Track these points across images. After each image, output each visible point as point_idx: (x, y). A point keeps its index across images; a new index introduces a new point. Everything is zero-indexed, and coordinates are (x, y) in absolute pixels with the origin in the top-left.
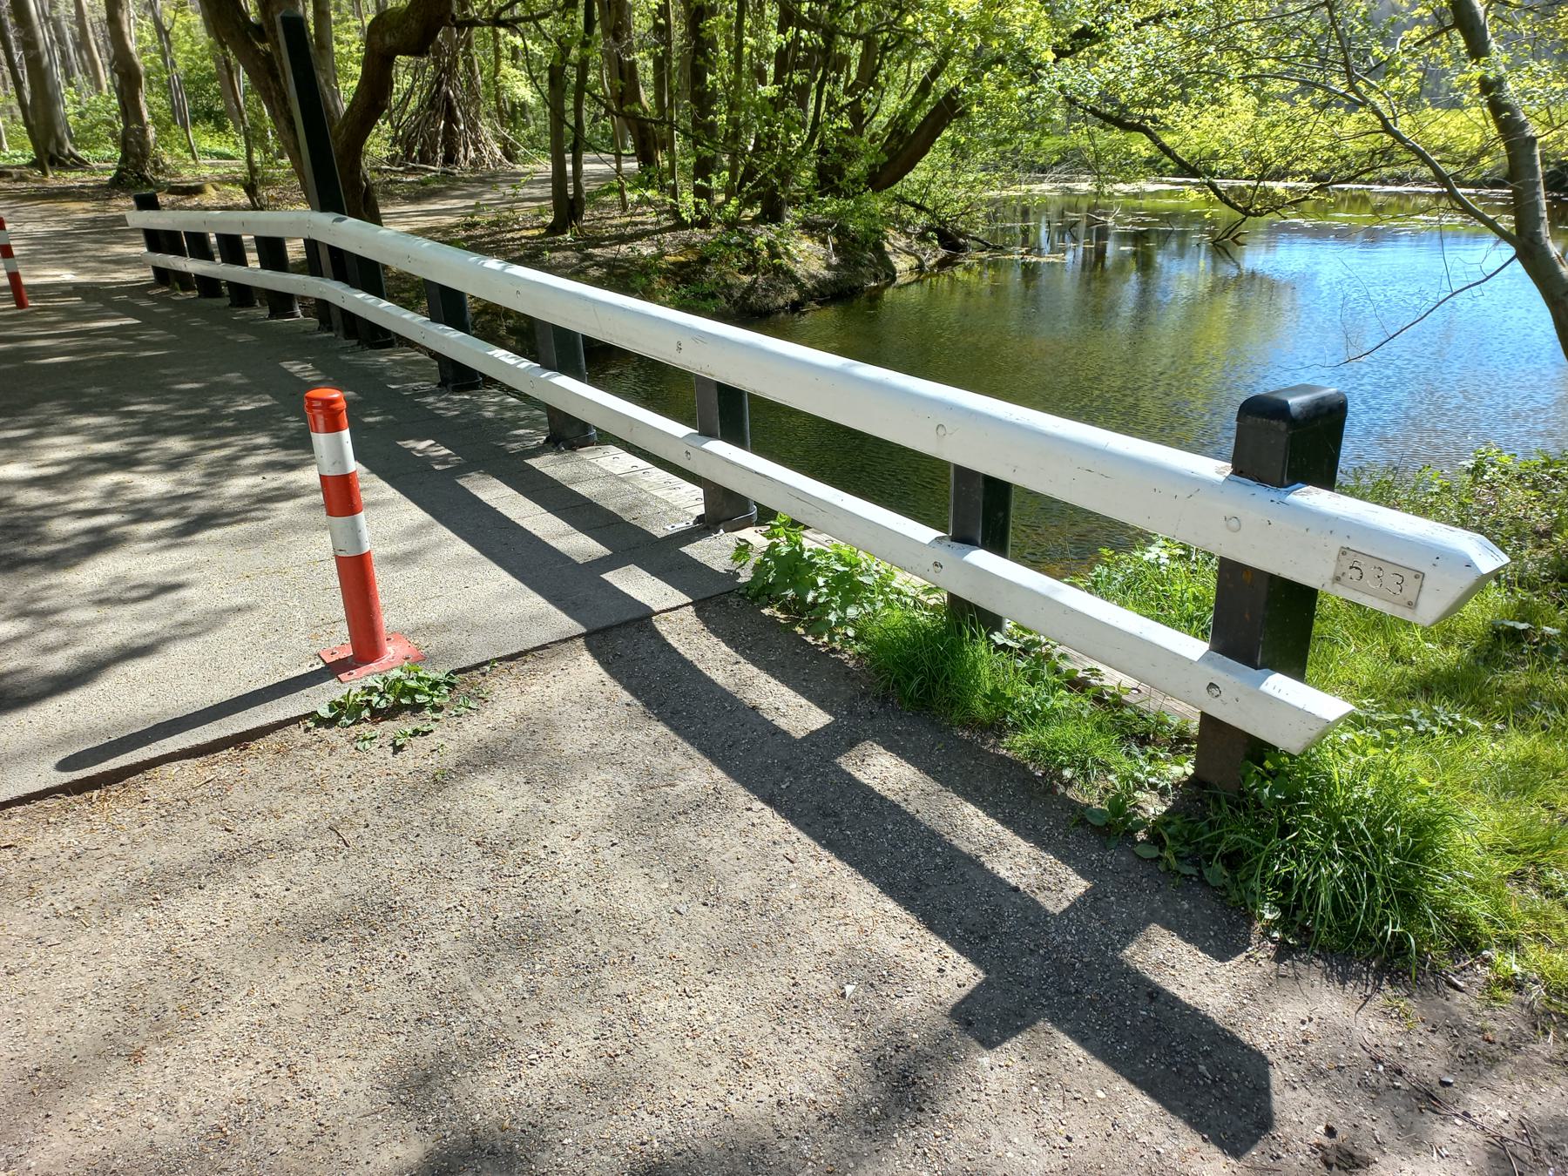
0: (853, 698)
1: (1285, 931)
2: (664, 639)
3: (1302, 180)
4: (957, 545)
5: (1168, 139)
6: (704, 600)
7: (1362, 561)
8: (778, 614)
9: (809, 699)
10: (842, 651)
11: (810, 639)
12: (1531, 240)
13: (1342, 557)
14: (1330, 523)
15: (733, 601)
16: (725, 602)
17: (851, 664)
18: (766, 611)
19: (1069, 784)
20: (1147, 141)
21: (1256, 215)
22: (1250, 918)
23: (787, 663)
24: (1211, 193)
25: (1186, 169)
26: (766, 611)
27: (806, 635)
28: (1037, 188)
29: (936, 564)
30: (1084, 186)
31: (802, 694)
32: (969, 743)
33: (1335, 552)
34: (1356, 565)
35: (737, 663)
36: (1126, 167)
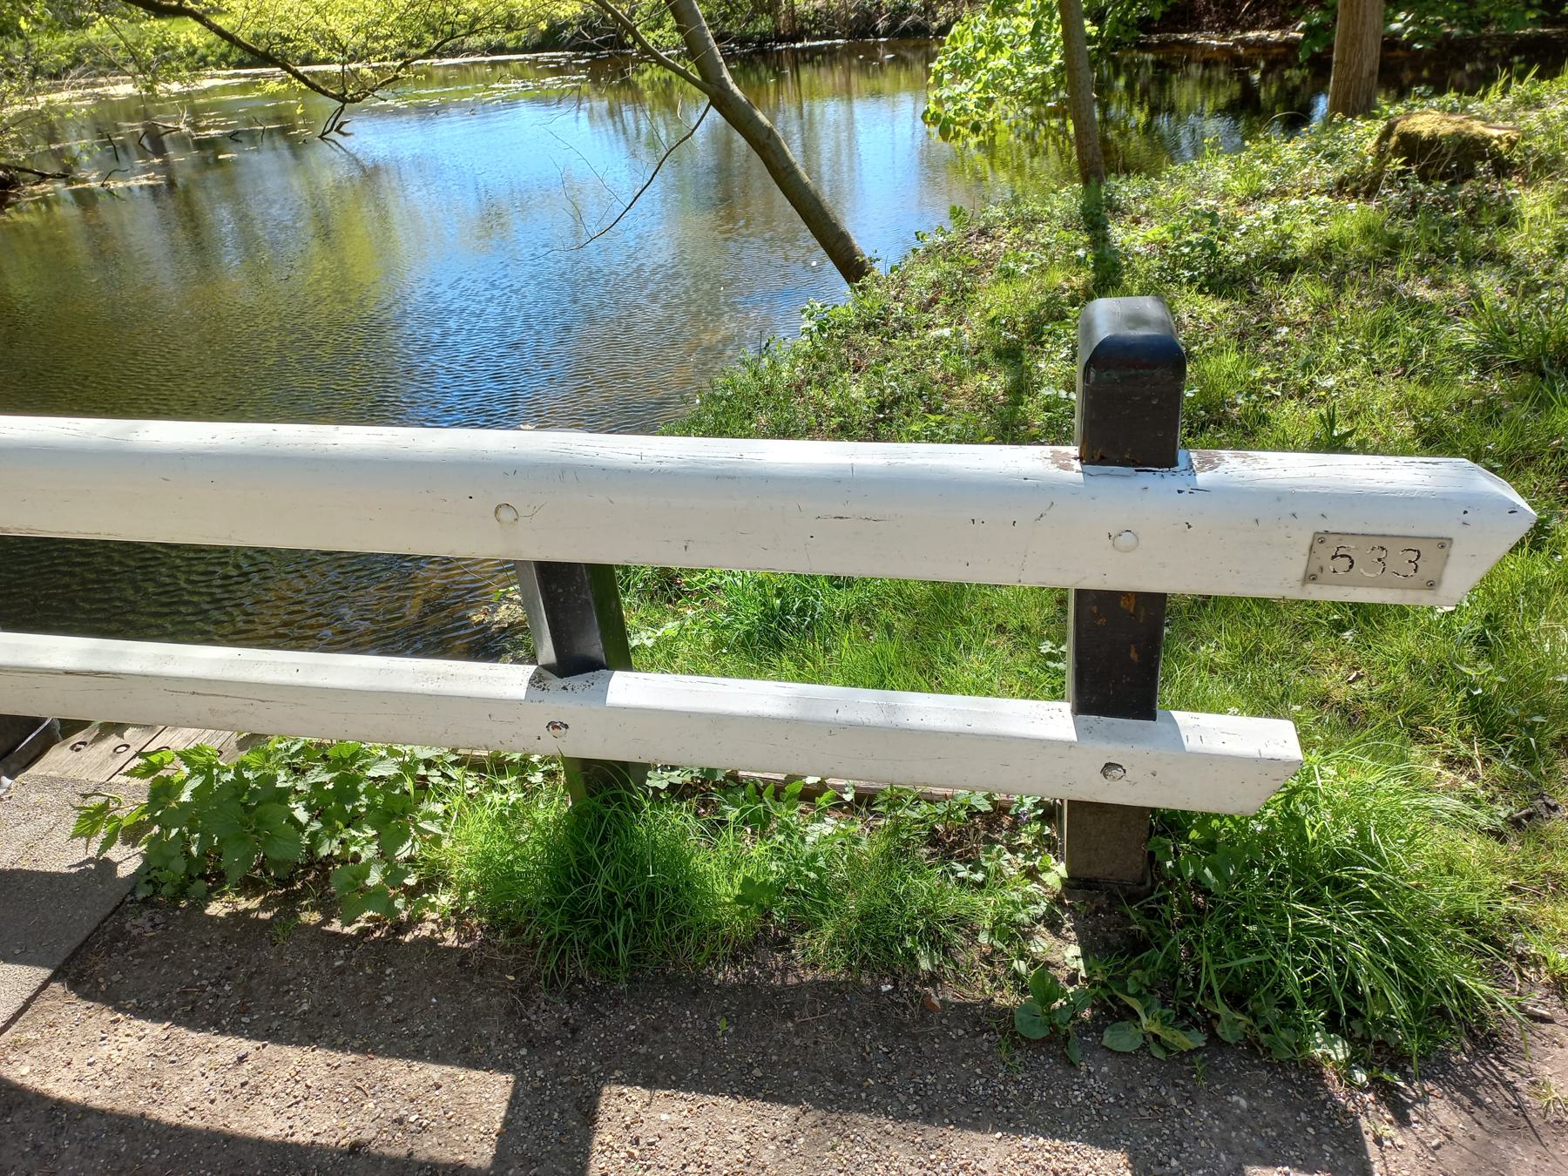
0: (511, 1012)
1: (1367, 1067)
2: (40, 1098)
3: (384, 59)
4: (577, 681)
5: (220, 21)
6: (75, 954)
7: (1351, 546)
8: (243, 904)
9: (439, 1059)
10: (415, 921)
11: (336, 926)
12: (721, 87)
13: (1317, 546)
14: (1284, 500)
15: (139, 924)
16: (121, 934)
17: (451, 938)
18: (216, 909)
19: (934, 979)
20: (197, 26)
21: (353, 101)
22: (1313, 1070)
23: (339, 1000)
24: (295, 81)
25: (258, 56)
26: (216, 909)
27: (327, 921)
28: (60, 98)
29: (553, 725)
30: (123, 89)
31: (418, 1055)
32: (749, 986)
33: (1307, 540)
34: (1341, 552)
35: (241, 1060)
36: (166, 59)
